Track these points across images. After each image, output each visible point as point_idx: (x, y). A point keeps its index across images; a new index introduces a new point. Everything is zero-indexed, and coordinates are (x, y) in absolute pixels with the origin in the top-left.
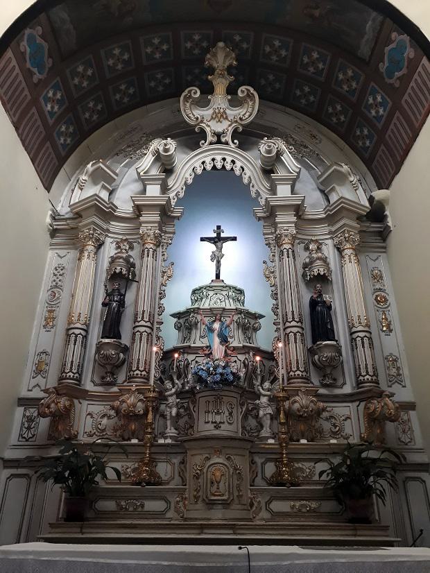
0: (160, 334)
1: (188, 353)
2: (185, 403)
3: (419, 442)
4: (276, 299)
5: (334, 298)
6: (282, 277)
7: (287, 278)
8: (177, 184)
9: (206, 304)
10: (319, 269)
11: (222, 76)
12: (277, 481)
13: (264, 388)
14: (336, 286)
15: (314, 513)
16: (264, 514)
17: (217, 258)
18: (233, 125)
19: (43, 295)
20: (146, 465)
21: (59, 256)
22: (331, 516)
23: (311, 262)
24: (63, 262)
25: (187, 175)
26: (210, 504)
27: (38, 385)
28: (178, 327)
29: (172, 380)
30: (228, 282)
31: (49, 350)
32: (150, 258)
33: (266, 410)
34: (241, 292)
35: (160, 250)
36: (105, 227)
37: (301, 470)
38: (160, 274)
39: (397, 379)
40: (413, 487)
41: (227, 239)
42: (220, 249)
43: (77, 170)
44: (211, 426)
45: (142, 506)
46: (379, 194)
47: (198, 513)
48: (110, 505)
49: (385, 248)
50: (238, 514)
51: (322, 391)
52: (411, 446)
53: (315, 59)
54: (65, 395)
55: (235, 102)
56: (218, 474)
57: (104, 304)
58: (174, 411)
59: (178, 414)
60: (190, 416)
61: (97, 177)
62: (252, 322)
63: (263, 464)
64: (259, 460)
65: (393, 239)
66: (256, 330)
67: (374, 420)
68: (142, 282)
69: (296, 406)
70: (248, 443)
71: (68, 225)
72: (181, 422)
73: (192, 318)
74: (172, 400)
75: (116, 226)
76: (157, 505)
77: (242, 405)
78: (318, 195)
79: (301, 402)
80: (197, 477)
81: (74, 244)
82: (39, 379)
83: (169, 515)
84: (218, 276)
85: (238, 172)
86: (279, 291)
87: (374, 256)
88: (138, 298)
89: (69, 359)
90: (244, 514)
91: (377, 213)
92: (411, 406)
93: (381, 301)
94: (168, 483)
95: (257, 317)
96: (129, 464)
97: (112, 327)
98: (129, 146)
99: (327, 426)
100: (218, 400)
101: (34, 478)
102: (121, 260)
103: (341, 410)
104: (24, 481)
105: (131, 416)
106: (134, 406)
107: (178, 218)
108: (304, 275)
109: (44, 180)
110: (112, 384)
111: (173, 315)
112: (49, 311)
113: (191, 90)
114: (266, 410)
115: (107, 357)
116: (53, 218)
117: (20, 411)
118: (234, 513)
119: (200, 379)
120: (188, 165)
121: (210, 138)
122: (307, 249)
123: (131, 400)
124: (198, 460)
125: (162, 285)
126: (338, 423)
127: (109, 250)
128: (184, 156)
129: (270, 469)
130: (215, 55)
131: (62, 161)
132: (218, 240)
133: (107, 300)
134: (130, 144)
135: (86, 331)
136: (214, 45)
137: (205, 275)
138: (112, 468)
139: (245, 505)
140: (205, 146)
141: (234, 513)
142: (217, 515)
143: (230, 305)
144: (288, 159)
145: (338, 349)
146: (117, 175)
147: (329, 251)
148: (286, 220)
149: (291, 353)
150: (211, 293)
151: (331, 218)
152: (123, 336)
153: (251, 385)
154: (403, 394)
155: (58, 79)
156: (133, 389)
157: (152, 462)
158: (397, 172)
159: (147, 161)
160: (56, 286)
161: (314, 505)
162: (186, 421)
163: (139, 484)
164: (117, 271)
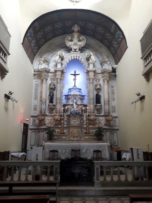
0: (62, 102)
1: (68, 105)
2: (68, 117)
3: (117, 125)
4: (88, 94)
5: (101, 94)
6: (90, 89)
7: (91, 89)
8: (65, 62)
9: (72, 93)
10: (98, 87)
11: (76, 33)
12: (86, 133)
13: (85, 115)
14: (102, 91)
15: (92, 138)
16: (83, 139)
17: (75, 80)
18: (79, 47)
19: (34, 91)
20: (62, 130)
21: (36, 81)
22: (95, 139)
23: (97, 85)
24: (37, 83)
25: (67, 60)
26: (74, 137)
27: (35, 113)
28: (66, 99)
29: (65, 113)
30: (78, 87)
31: (37, 105)
32: (59, 84)
33: (85, 119)
34: (80, 89)
35: (61, 81)
36: (47, 75)
37: (91, 131)
38: (61, 87)
39: (114, 111)
41: (77, 75)
42: (75, 77)
43: (38, 56)
44: (73, 122)
45: (62, 137)
46: (115, 66)
47: (72, 138)
48: (56, 137)
49: (115, 79)
50: (79, 139)
51: (97, 114)
52: (115, 125)
53: (100, 30)
54: (43, 116)
55: (79, 41)
56: (75, 132)
57: (49, 95)
58: (66, 119)
59: (67, 120)
60: (69, 120)
61: (45, 61)
62: (83, 97)
63: (84, 130)
64: (83, 129)
65: (117, 78)
66: (84, 99)
67: (107, 121)
68: (58, 90)
69: (91, 118)
70: (80, 126)
71: (37, 73)
72: (67, 121)
73: (69, 97)
74: (66, 117)
75: (50, 74)
77: (80, 118)
78: (100, 66)
79: (92, 117)
80: (72, 132)
81: (39, 78)
82: (35, 111)
83: (67, 139)
85: (80, 60)
86: (89, 92)
87: (113, 81)
88: (57, 94)
89: (43, 108)
90: (80, 139)
91: (114, 70)
92: (116, 117)
93: (113, 93)
94: (66, 133)
95: (84, 96)
96: (59, 130)
97: (51, 101)
98: (51, 50)
99: (98, 122)
100: (75, 117)
101: (37, 133)
102: (52, 85)
103: (101, 118)
104: (35, 133)
105: (57, 120)
106: (58, 118)
107: (65, 72)
108: (95, 88)
109: (25, 49)
110: (52, 113)
111: (64, 95)
112: (35, 96)
113: (69, 37)
114: (85, 119)
115: (51, 108)
116: (34, 71)
118: (78, 138)
119: (71, 113)
120: (68, 57)
121: (73, 50)
122: (96, 81)
123: (57, 117)
124: (72, 130)
125: (62, 90)
126: (100, 121)
127: (49, 81)
128: (66, 54)
129: (85, 131)
130: (74, 27)
131: (35, 55)
132: (75, 75)
133: (50, 94)
134: (52, 49)
135: (45, 101)
136: (74, 25)
137: (71, 85)
140: (72, 52)
141: (78, 138)
142: (75, 139)
143: (78, 93)
144: (93, 58)
145: (101, 106)
146: (49, 60)
147: (101, 82)
148: (91, 74)
149: (91, 107)
150: (73, 90)
151: (103, 73)
152: (54, 103)
153: (82, 113)
154: (114, 115)
155: (35, 38)
156: (58, 115)
157: (63, 130)
158: (119, 62)
159: (57, 58)
160: (36, 89)
161: (92, 137)
162: (68, 122)
163: (61, 134)
164: (52, 87)
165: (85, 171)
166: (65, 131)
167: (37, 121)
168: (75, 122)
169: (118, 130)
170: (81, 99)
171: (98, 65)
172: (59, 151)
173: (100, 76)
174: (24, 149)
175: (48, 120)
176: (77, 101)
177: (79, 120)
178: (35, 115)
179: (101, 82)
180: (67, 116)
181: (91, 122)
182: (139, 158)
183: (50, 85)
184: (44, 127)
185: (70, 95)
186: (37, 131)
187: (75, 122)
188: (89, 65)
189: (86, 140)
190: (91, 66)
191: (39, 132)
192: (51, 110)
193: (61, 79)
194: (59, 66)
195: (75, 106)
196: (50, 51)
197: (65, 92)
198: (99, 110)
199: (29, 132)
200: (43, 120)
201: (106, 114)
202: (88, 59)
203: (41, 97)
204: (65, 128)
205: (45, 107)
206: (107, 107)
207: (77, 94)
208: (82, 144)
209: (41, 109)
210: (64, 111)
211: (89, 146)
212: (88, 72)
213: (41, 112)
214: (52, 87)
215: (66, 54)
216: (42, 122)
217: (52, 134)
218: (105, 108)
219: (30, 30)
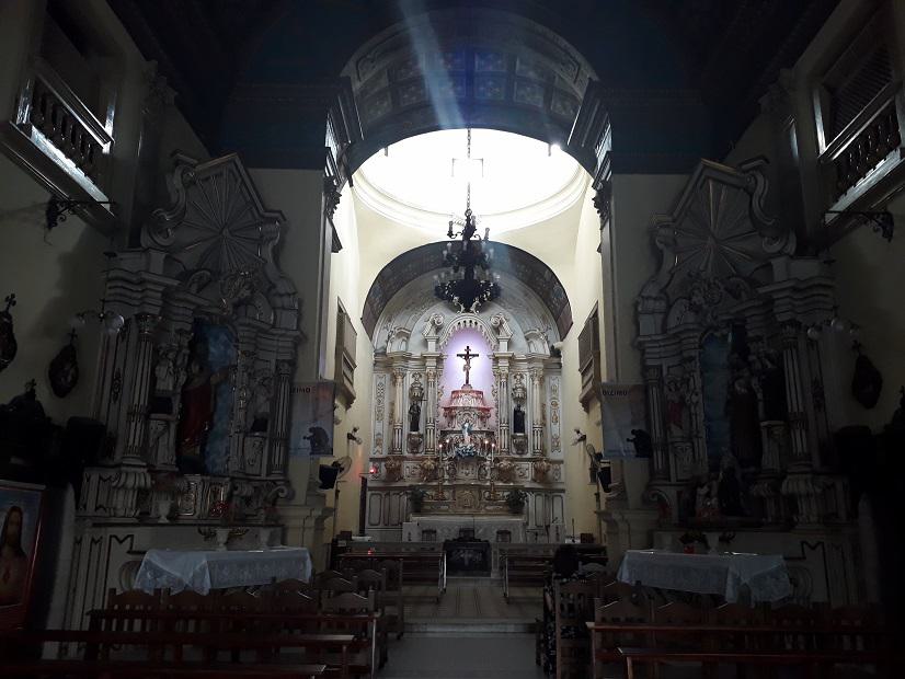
9: (460, 403)
10: (519, 393)
12: (489, 499)
13: (490, 457)
17: (467, 369)
23: (516, 388)
24: (383, 381)
34: (481, 393)
39: (557, 448)
40: (557, 500)
41: (474, 356)
42: (468, 363)
46: (557, 345)
51: (517, 456)
79: (504, 463)
84: (467, 382)
87: (554, 377)
88: (428, 411)
95: (488, 410)
97: (415, 426)
100: (467, 464)
122: (515, 377)
127: (410, 380)
132: (467, 357)
139: (622, 461)
142: (467, 511)
143: (473, 403)
145: (526, 437)
148: (504, 364)
154: (553, 456)
162: (453, 475)
165: (478, 557)
166: (446, 494)
167: (383, 470)
168: (467, 475)
169: (563, 491)
170: (482, 418)
171: (520, 342)
172: (439, 531)
173: (524, 367)
175: (408, 468)
176: (470, 426)
177: (476, 469)
178: (378, 456)
179: (526, 382)
180: (450, 459)
181: (506, 475)
182: (115, 397)
183: (412, 389)
185: (456, 408)
188: (498, 341)
190: (504, 345)
192: (415, 446)
194: (432, 345)
195: (467, 437)
197: (445, 399)
198: (521, 448)
201: (538, 456)
202: (497, 329)
205: (402, 439)
206: (538, 439)
207: (473, 405)
208: (478, 519)
210: (447, 448)
212: (496, 360)
213: (392, 450)
215: (447, 316)
216: (394, 473)
218: (534, 441)
219: (376, 285)
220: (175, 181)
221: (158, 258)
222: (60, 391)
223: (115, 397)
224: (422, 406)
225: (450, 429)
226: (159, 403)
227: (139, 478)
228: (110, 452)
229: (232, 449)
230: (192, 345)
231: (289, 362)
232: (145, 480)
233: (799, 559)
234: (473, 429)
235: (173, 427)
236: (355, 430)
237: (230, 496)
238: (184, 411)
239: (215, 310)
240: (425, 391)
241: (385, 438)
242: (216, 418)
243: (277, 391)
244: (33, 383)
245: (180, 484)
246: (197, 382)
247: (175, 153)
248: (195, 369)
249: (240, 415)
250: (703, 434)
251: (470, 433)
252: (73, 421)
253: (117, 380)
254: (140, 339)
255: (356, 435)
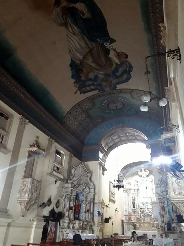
19: (124, 201)
47: (146, 229)
76: (142, 228)
82: (126, 212)
97: (134, 207)
100: (147, 217)
105: (138, 218)
117: (125, 216)
127: (132, 195)
138: (6, 131)
142: (147, 229)
157: (141, 224)
162: (144, 220)
166: (142, 225)
168: (147, 220)
174: (123, 234)
175: (133, 218)
178: (126, 214)
182: (64, 207)
184: (131, 222)
186: (128, 224)
187: (147, 220)
189: (152, 230)
191: (129, 224)
192: (134, 212)
193: (137, 194)
195: (147, 210)
196: (130, 176)
199: (124, 224)
200: (131, 218)
203: (128, 204)
204: (142, 223)
209: (129, 211)
211: (150, 233)
214: (133, 198)
216: (130, 219)
217: (135, 226)
220: (73, 171)
221: (70, 185)
222: (57, 207)
223: (64, 207)
224: (135, 202)
225: (143, 207)
226: (71, 208)
227: (68, 221)
228: (64, 217)
229: (83, 215)
230: (76, 198)
231: (93, 199)
232: (69, 222)
233: (177, 240)
234: (148, 207)
235: (73, 212)
236: (117, 209)
237: (83, 224)
238: (75, 209)
239: (79, 191)
240: (135, 198)
241: (127, 209)
242: (81, 210)
243: (91, 205)
244: (53, 207)
245: (74, 222)
246: (77, 204)
247: (73, 166)
248: (77, 201)
249: (84, 209)
250: (168, 213)
251: (148, 209)
252: (59, 212)
253: (65, 204)
254: (68, 198)
255: (117, 210)
